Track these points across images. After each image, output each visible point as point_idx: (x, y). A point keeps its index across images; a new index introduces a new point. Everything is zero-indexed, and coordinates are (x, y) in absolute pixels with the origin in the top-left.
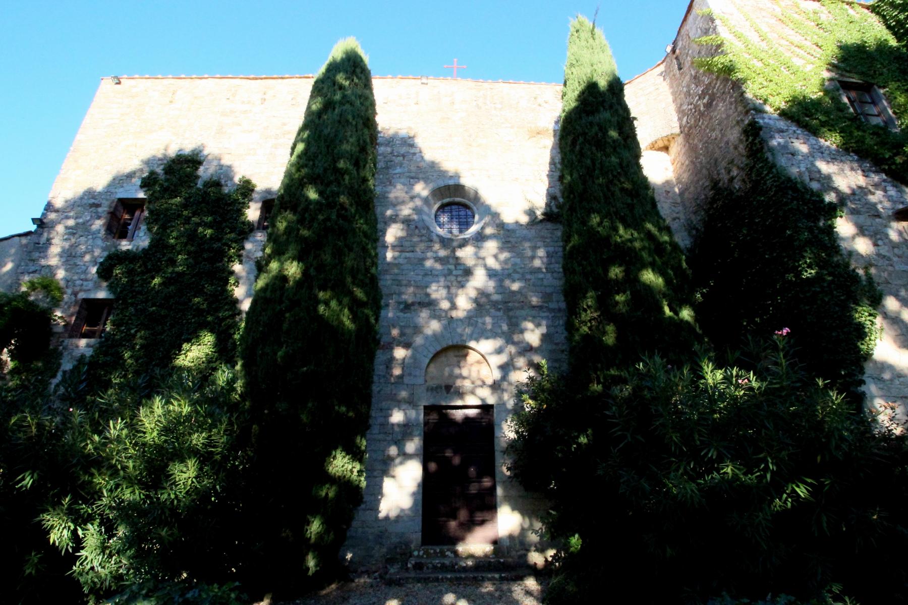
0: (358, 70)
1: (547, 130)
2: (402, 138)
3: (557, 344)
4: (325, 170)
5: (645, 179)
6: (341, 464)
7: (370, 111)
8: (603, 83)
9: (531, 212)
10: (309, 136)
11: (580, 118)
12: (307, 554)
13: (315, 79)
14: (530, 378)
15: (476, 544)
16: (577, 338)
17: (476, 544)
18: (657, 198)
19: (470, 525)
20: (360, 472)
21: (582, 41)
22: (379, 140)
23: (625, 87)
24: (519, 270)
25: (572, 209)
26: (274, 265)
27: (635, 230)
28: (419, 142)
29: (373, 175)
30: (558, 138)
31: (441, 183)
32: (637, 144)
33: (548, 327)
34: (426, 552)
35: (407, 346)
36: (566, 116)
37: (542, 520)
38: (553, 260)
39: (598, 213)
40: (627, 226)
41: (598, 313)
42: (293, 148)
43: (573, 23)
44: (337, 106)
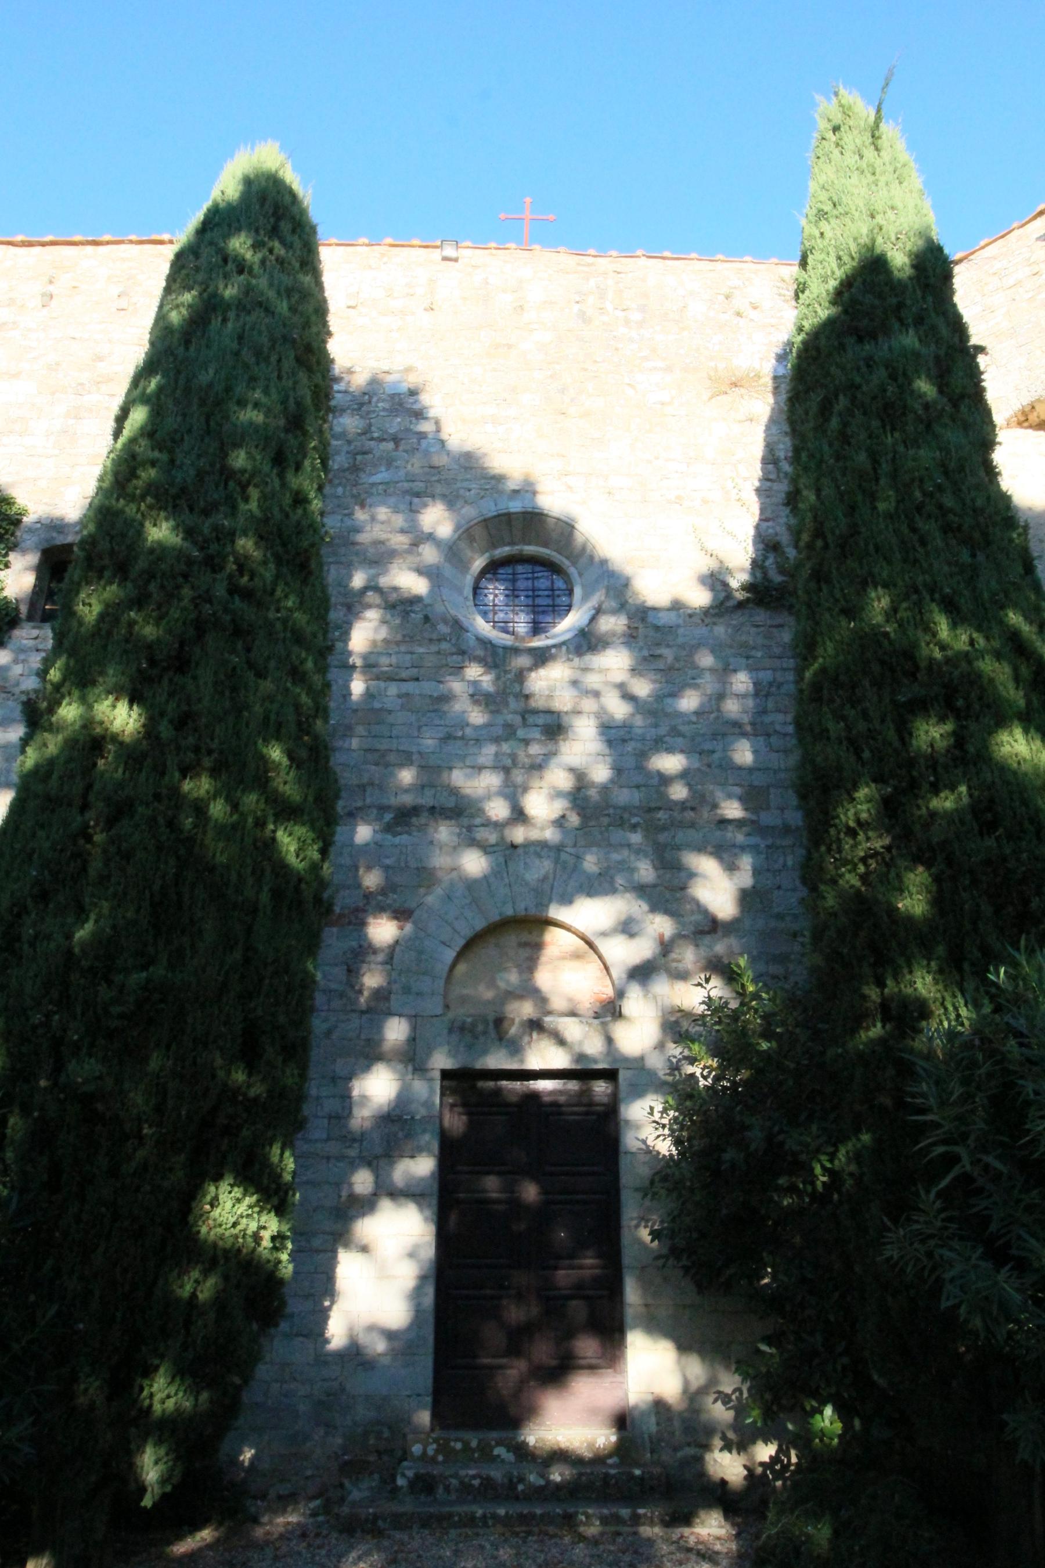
0: (285, 226)
1: (758, 376)
2: (393, 396)
3: (779, 917)
4: (200, 475)
5: (1005, 499)
6: (232, 1212)
7: (314, 330)
8: (899, 259)
9: (715, 580)
10: (160, 389)
11: (842, 347)
12: (141, 1450)
13: (175, 248)
14: (709, 1001)
15: (572, 1422)
16: (830, 901)
17: (572, 1422)
18: (1036, 548)
19: (558, 1372)
20: (278, 1239)
21: (848, 154)
22: (338, 399)
23: (957, 270)
24: (683, 728)
25: (819, 576)
26: (69, 712)
27: (979, 629)
28: (433, 402)
29: (320, 489)
30: (784, 397)
31: (490, 508)
32: (987, 412)
33: (756, 872)
34: (444, 1448)
35: (400, 914)
36: (804, 343)
37: (741, 1367)
38: (770, 705)
39: (885, 586)
40: (957, 617)
41: (887, 841)
42: (121, 418)
43: (827, 108)
44: (231, 315)
